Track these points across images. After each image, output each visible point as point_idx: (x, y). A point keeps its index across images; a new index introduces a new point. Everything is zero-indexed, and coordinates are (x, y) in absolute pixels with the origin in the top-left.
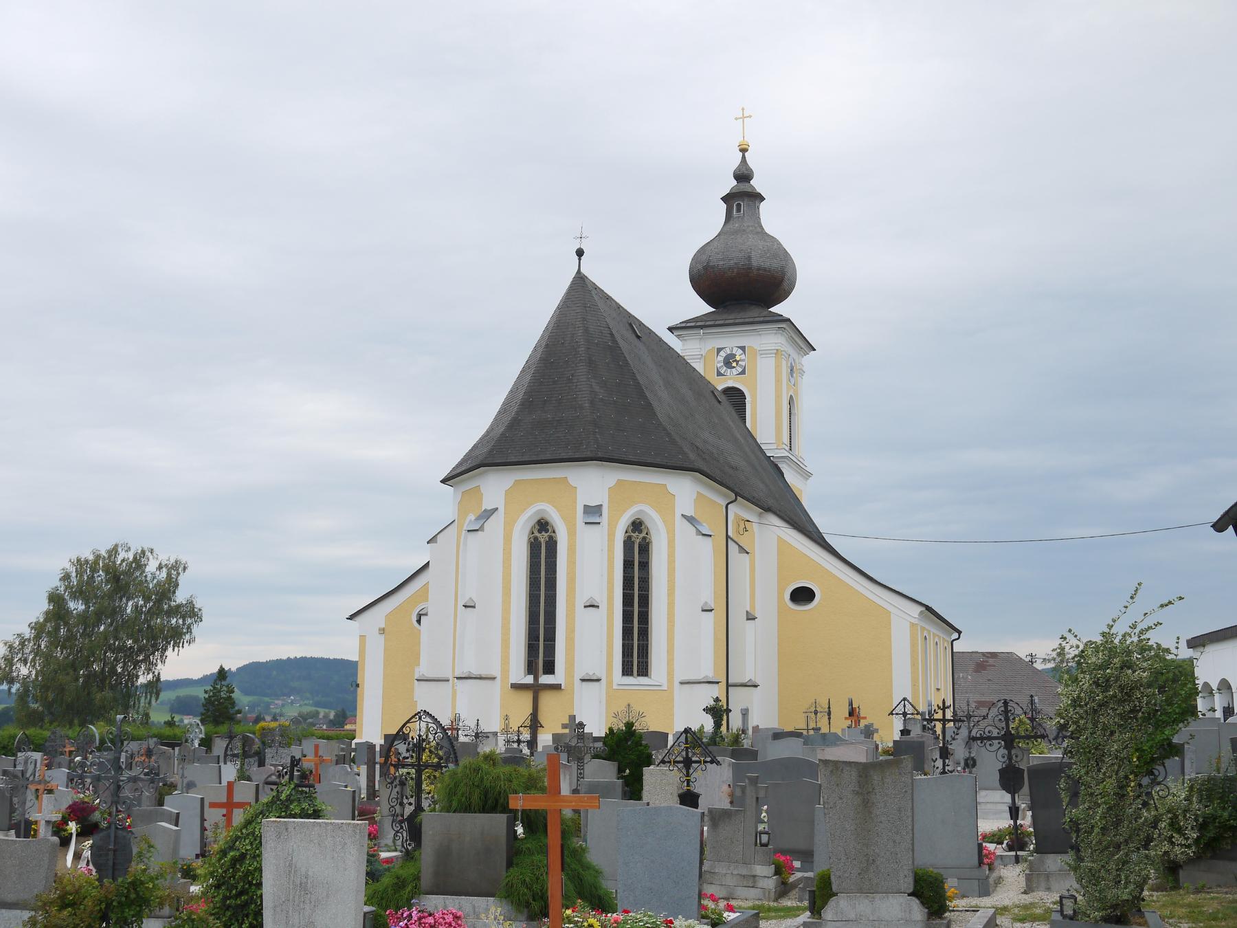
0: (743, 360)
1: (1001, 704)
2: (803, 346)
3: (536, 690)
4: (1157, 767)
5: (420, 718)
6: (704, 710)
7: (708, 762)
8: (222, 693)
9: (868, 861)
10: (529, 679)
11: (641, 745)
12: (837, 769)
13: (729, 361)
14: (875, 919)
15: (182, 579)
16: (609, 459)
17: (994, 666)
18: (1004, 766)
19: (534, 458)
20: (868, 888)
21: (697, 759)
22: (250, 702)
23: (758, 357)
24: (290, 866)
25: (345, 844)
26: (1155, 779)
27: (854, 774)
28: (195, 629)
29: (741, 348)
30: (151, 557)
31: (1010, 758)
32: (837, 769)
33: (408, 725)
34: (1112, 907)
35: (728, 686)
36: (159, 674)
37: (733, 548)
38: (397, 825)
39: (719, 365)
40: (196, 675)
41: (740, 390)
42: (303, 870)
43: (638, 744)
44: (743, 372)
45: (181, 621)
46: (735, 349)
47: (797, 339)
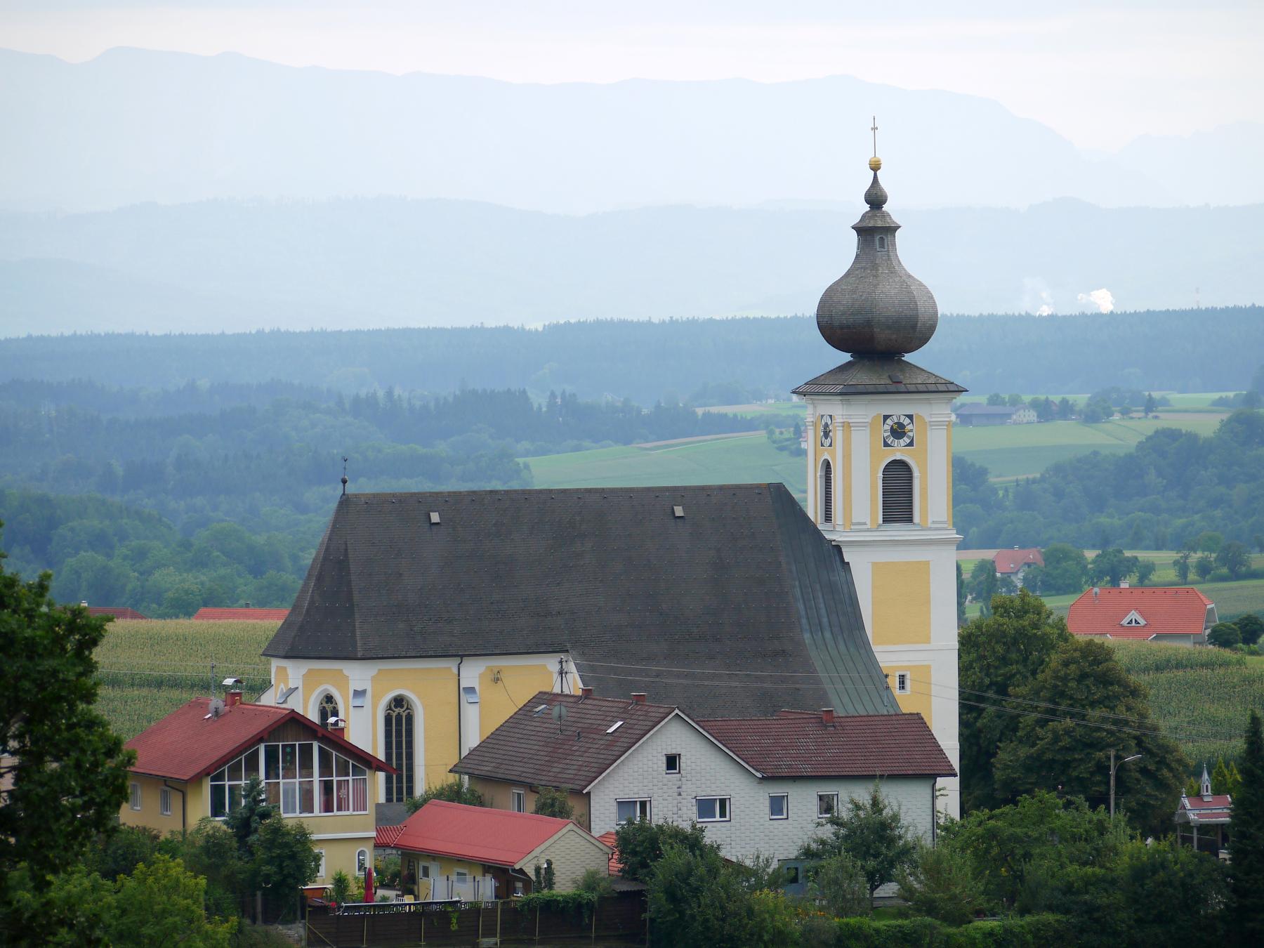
0: (911, 431)
23: (928, 428)
39: (886, 434)
44: (911, 444)
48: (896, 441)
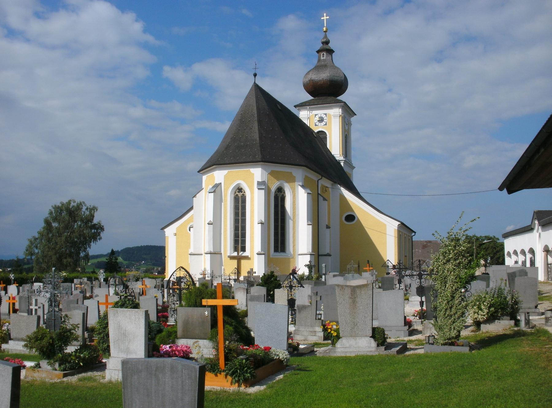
0: (326, 119)
1: (418, 261)
3: (239, 259)
4: (468, 285)
5: (180, 270)
9: (354, 324)
10: (235, 254)
12: (343, 288)
13: (321, 120)
15: (96, 214)
19: (236, 161)
20: (354, 335)
21: (295, 285)
22: (126, 263)
26: (467, 290)
27: (349, 290)
28: (102, 235)
29: (325, 114)
30: (83, 205)
31: (421, 283)
32: (343, 288)
33: (175, 272)
34: (448, 339)
35: (319, 255)
36: (88, 252)
37: (321, 199)
39: (316, 121)
40: (105, 253)
41: (324, 132)
43: (276, 280)
45: (95, 231)
46: (322, 115)
47: (347, 109)
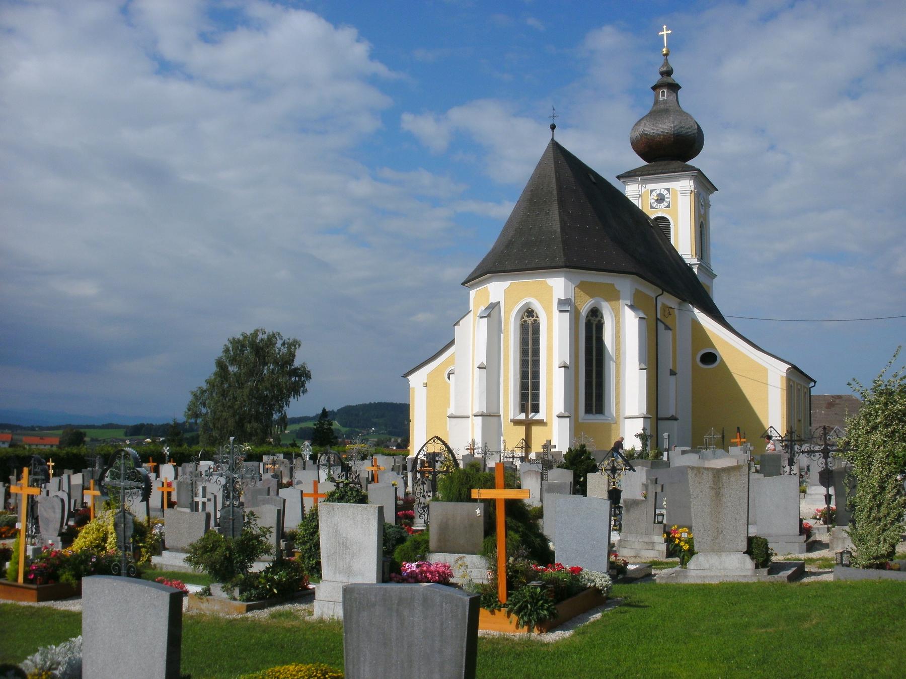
0: (669, 198)
2: (709, 188)
3: (528, 425)
5: (434, 441)
6: (635, 436)
7: (627, 469)
8: (325, 426)
9: (718, 531)
10: (522, 416)
11: (590, 459)
14: (721, 568)
16: (574, 267)
17: (840, 404)
18: (822, 469)
19: (524, 267)
20: (717, 549)
24: (336, 532)
25: (369, 519)
27: (710, 475)
31: (826, 464)
34: (874, 558)
36: (285, 413)
37: (661, 326)
38: (421, 509)
39: (652, 201)
42: (344, 535)
43: (588, 458)
45: (297, 379)
46: (663, 190)
48: (659, 205)
